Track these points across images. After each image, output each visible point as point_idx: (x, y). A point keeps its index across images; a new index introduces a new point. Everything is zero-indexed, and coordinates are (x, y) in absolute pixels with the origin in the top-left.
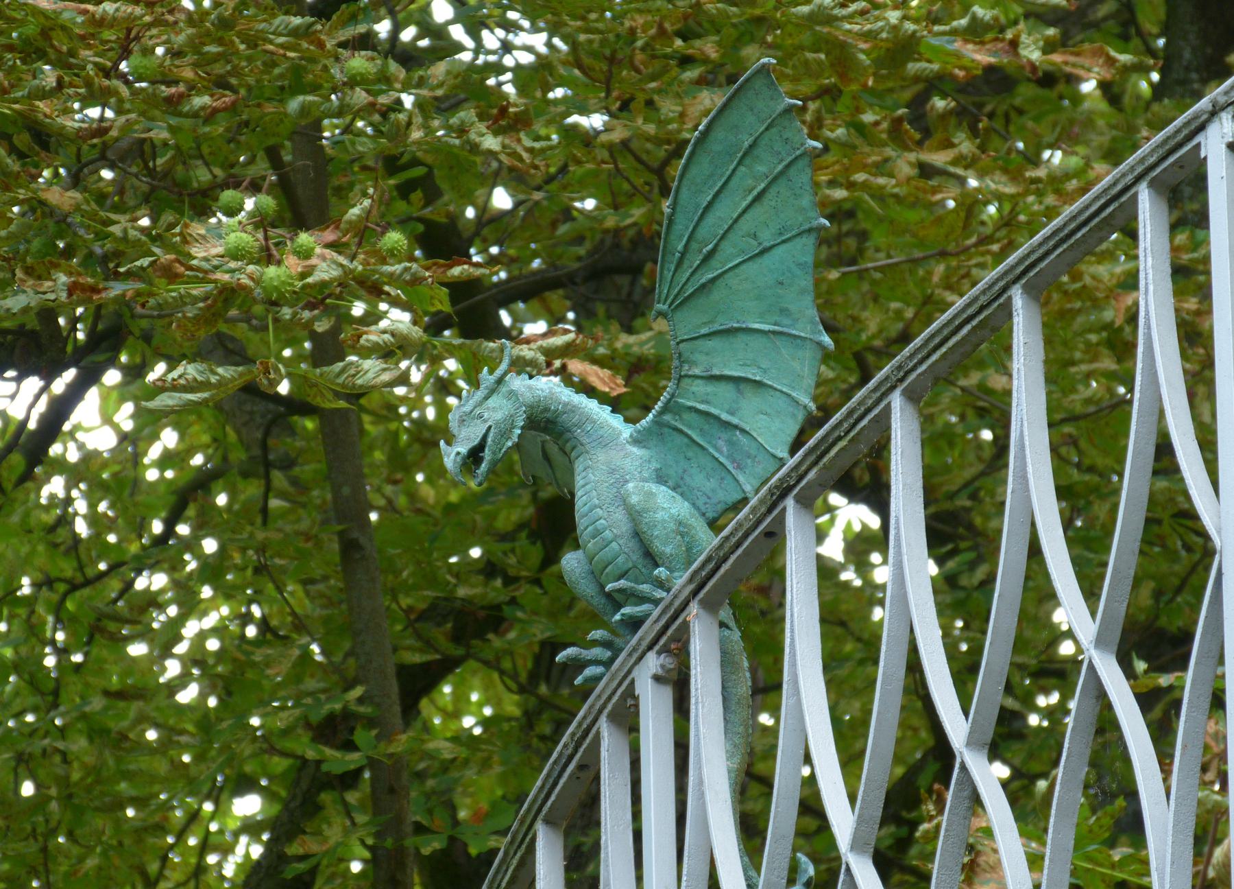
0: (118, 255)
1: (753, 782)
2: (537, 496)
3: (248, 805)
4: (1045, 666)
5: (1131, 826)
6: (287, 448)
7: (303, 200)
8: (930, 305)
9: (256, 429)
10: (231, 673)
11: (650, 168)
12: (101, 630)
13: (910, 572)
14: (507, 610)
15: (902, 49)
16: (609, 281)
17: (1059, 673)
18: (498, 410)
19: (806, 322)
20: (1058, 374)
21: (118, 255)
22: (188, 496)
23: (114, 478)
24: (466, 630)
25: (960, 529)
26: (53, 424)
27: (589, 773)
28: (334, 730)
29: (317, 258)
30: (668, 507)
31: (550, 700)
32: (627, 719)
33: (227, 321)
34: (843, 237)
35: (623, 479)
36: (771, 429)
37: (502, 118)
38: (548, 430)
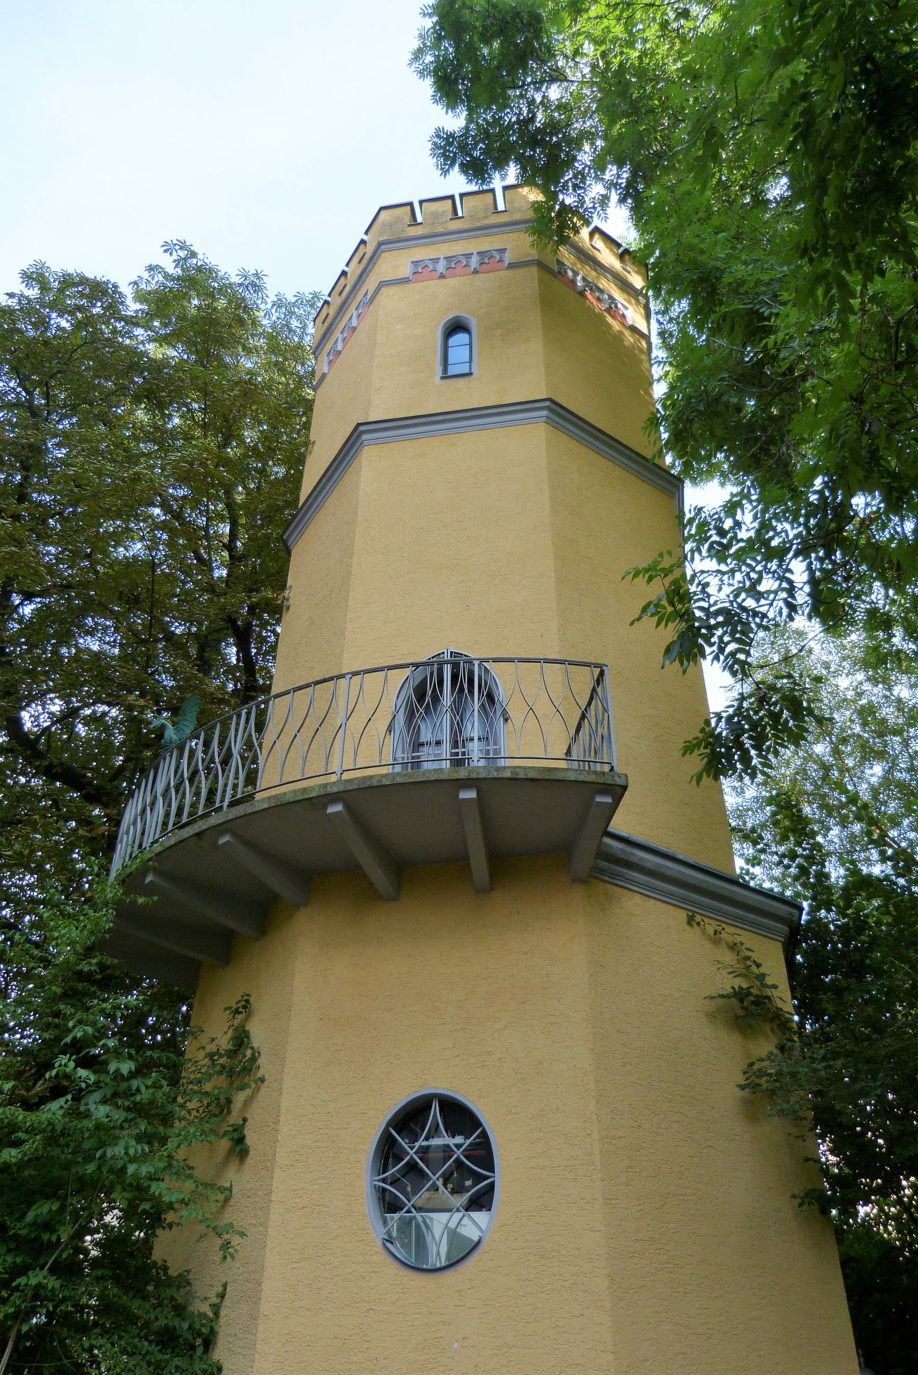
0: (791, 369)
1: (177, 768)
2: (160, 732)
3: (121, 758)
4: (212, 761)
5: (217, 782)
6: (133, 723)
7: (142, 696)
8: (210, 721)
9: (131, 720)
10: (123, 743)
11: (182, 700)
12: (109, 736)
13: (200, 747)
14: (752, 49)
15: (213, 694)
16: (175, 711)
17: (214, 763)
18: (158, 723)
19: (195, 721)
20: (221, 731)
21: (791, 369)
22: (122, 723)
23: (114, 719)
24: (148, 746)
25: (207, 745)
26: (109, 712)
27: (159, 764)
28: (132, 752)
29: (142, 702)
30: (175, 737)
31: (156, 756)
32: (165, 759)
33: (130, 708)
34: (202, 712)
35: (170, 733)
36: (188, 731)
37: (166, 692)
38: (163, 727)
